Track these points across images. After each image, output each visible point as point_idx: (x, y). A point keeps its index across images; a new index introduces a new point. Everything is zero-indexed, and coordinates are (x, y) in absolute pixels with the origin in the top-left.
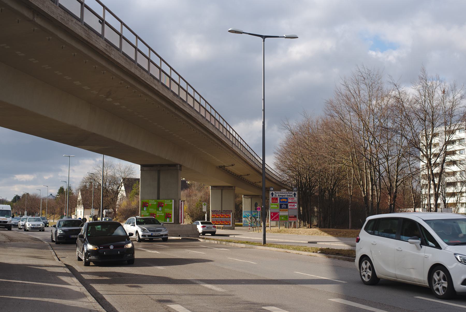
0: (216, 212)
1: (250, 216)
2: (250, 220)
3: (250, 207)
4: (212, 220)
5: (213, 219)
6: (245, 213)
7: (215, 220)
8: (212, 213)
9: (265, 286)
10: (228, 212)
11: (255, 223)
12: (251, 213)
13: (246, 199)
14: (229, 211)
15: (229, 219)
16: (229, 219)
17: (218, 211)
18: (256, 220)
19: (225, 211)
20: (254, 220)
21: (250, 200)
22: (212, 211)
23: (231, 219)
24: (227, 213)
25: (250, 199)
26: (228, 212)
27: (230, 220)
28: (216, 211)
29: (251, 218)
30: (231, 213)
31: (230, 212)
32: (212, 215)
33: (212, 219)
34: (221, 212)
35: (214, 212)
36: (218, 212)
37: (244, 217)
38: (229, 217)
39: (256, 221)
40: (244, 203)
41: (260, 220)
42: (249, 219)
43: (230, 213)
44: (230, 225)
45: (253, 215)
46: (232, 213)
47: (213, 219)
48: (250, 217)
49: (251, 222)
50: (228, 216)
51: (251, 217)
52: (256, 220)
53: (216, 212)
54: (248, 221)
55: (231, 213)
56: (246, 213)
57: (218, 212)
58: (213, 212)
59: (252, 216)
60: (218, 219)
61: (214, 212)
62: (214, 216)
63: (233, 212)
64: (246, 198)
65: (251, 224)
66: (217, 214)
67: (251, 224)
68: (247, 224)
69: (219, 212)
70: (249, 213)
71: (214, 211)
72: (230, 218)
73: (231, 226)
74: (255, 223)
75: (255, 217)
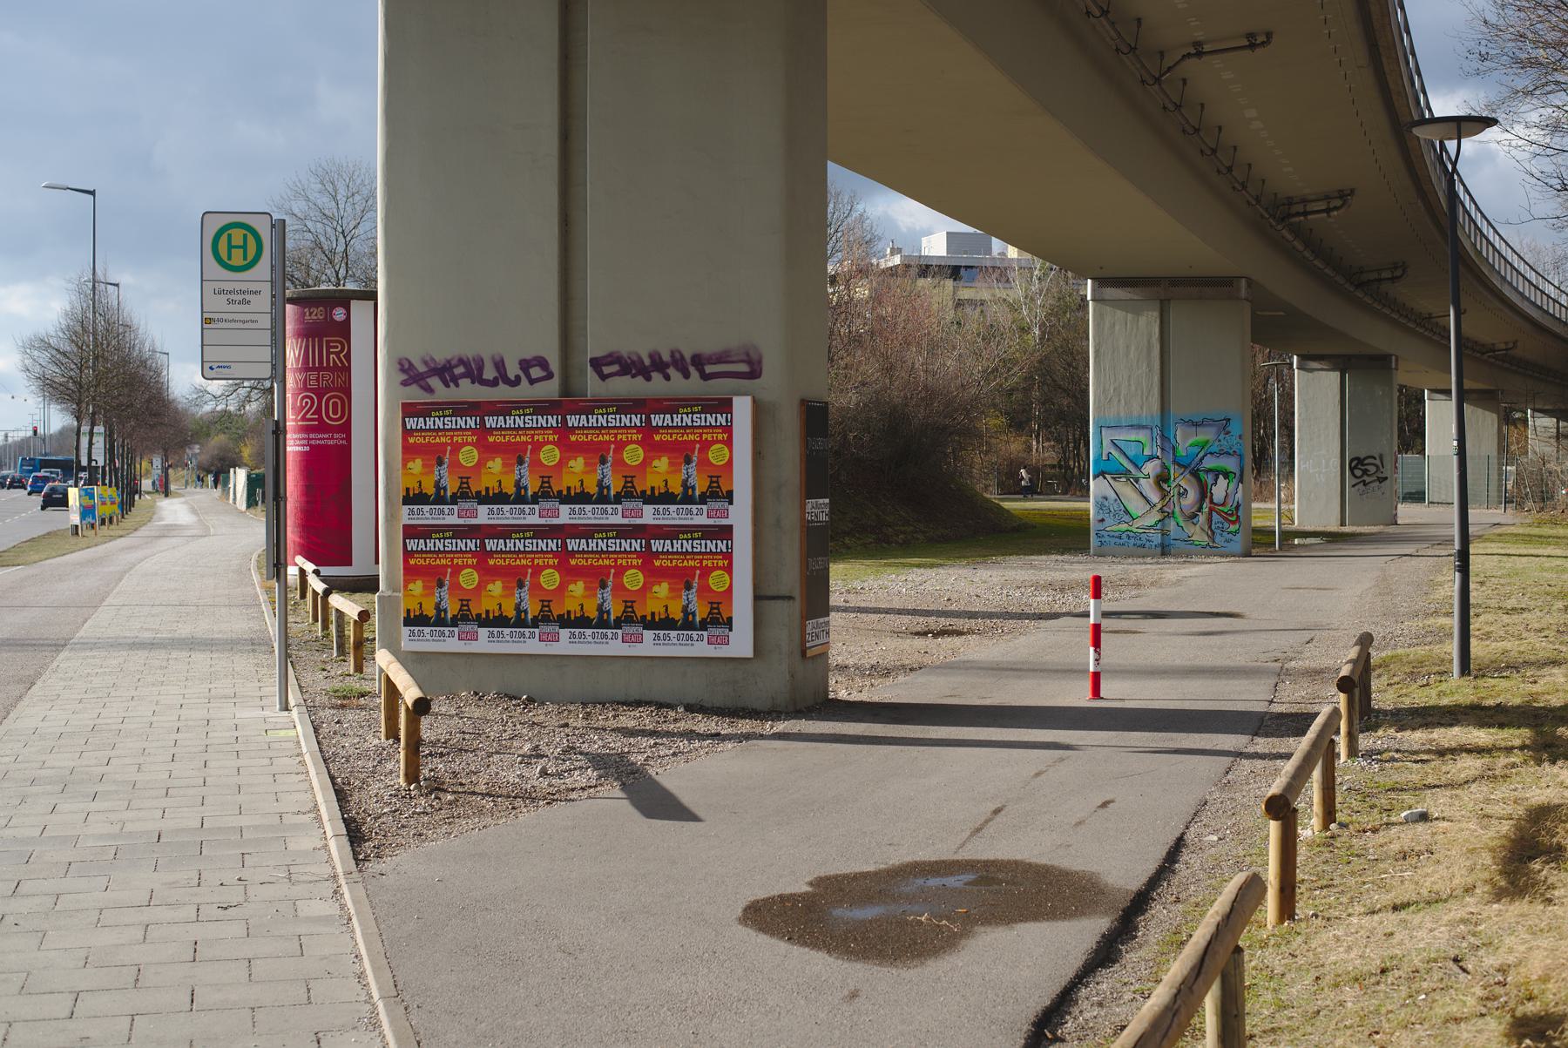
0: (467, 391)
1: (1151, 458)
2: (1155, 497)
3: (1156, 379)
4: (411, 532)
5: (427, 515)
6: (1107, 436)
7: (623, 532)
8: (410, 410)
9: (1201, 620)
10: (677, 385)
11: (1202, 518)
12: (1164, 437)
13: (1120, 314)
14: (699, 361)
15: (699, 516)
16: (699, 516)
17: (500, 365)
18: (1204, 492)
19: (629, 367)
20: (1192, 495)
21: (1149, 321)
22: (409, 374)
23: (740, 516)
24: (504, 409)
25: (1156, 314)
26: (677, 385)
27: (725, 533)
28: (474, 372)
29: (1162, 479)
30: (742, 408)
31: (717, 388)
32: (410, 451)
33: (405, 515)
34: (549, 389)
35: (442, 393)
36: (502, 393)
37: (1101, 474)
38: (700, 484)
39: (1206, 506)
40: (1097, 352)
41: (1239, 495)
42: (1147, 486)
43: (725, 406)
44: (718, 620)
45: (1181, 452)
46: (759, 410)
47: (427, 515)
48: (1151, 468)
49: (1167, 515)
50: (681, 452)
51: (1164, 466)
52: (1204, 492)
53: (467, 391)
54: (1135, 505)
55: (742, 408)
56: (1122, 436)
57: (502, 393)
58: (415, 395)
59: (1175, 462)
60: (589, 515)
61: (442, 393)
62: (436, 455)
63: (772, 382)
64: (1116, 303)
65: (1164, 533)
66: (482, 431)
67: (1164, 533)
68: (1124, 527)
69: (524, 391)
70: (1143, 436)
71: (445, 372)
72: (719, 493)
73: (740, 642)
74: (1202, 518)
75: (1195, 474)
